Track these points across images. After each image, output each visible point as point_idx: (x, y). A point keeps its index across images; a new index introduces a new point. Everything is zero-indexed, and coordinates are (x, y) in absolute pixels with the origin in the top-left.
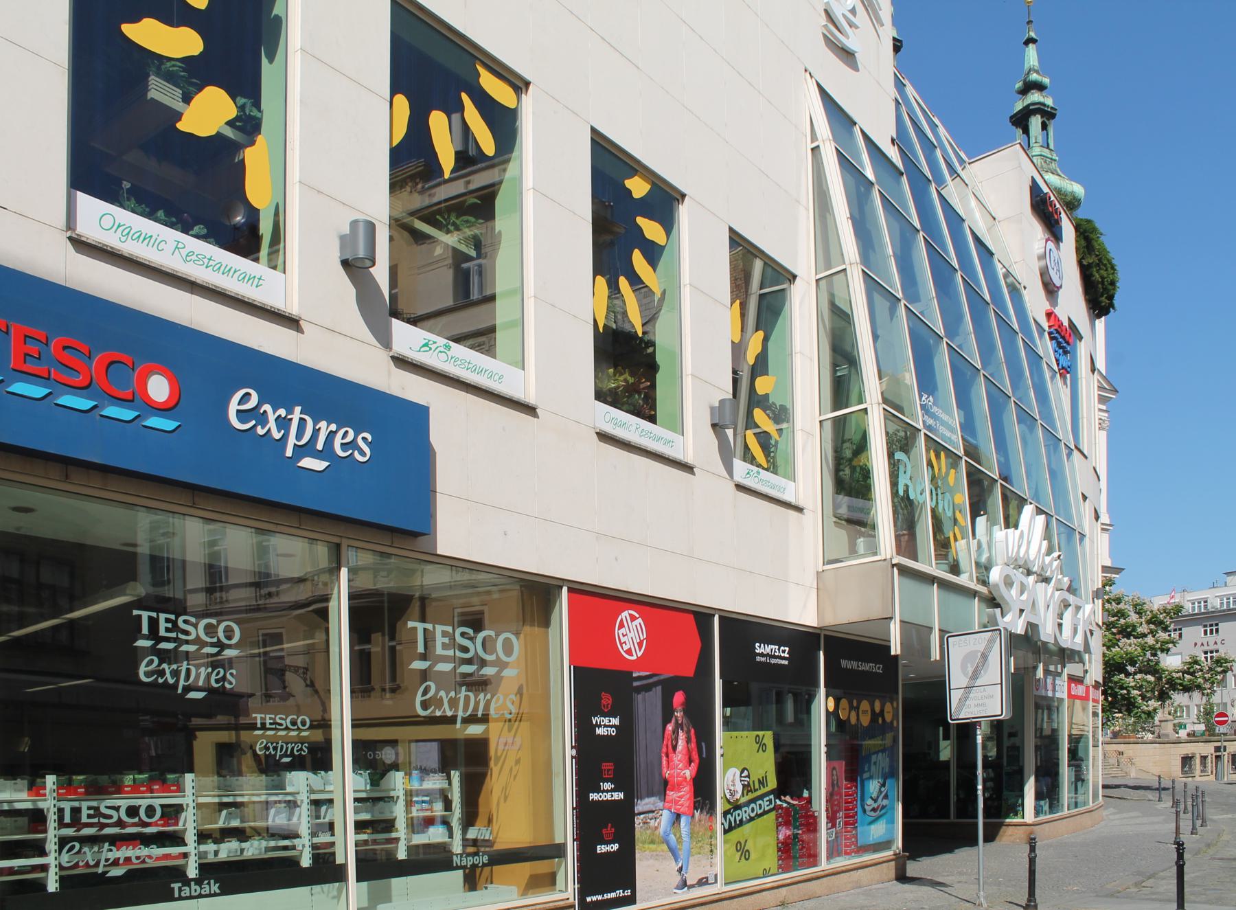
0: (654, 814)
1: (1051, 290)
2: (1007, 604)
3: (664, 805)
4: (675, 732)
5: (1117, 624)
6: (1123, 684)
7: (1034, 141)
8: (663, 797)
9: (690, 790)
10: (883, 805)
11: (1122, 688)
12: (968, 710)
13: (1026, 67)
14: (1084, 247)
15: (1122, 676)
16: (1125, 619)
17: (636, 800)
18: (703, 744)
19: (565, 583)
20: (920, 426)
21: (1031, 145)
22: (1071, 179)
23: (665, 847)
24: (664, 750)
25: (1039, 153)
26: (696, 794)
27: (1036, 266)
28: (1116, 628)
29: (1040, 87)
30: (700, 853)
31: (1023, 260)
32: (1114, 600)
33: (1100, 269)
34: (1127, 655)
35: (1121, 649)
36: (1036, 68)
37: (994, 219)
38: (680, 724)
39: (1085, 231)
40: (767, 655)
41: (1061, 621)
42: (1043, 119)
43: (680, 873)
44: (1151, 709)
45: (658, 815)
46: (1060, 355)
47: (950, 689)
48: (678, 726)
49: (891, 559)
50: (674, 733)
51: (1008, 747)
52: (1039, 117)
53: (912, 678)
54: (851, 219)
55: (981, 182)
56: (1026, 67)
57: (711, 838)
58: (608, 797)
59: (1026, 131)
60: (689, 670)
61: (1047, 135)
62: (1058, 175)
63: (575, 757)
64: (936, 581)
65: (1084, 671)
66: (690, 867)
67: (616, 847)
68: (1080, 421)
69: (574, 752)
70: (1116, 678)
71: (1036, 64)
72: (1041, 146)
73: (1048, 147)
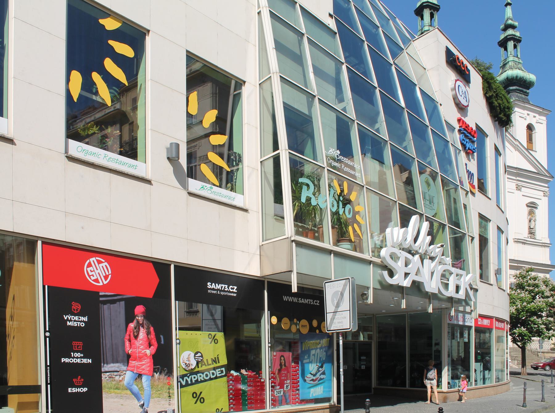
0: (118, 373)
1: (462, 108)
2: (394, 269)
3: (127, 368)
4: (137, 328)
5: (534, 291)
6: (536, 322)
7: (510, 54)
8: (127, 364)
9: (150, 361)
10: (320, 378)
11: (535, 324)
12: (335, 325)
13: (506, 17)
14: (487, 87)
15: (535, 317)
16: (538, 289)
17: (102, 364)
18: (162, 337)
19: (39, 238)
20: (325, 165)
21: (508, 56)
22: (529, 72)
23: (129, 392)
24: (127, 337)
25: (512, 60)
26: (155, 364)
27: (450, 94)
28: (534, 293)
29: (513, 27)
30: (159, 397)
31: (440, 90)
32: (533, 279)
33: (498, 99)
34: (537, 307)
35: (535, 303)
36: (511, 17)
37: (425, 69)
38: (141, 324)
39: (487, 79)
40: (218, 290)
41: (448, 282)
42: (514, 43)
43: (142, 407)
44: (550, 335)
45: (122, 374)
46: (467, 142)
47: (326, 313)
48: (139, 325)
49: (291, 237)
50: (135, 328)
51: (435, 351)
52: (512, 42)
53: (384, 313)
54: (275, 49)
55: (419, 50)
56: (506, 17)
57: (169, 389)
58: (78, 361)
59: (506, 49)
60: (149, 293)
61: (517, 50)
62: (522, 70)
63: (270, 347)
64: (332, 252)
65: (471, 310)
66: (150, 405)
67: (85, 389)
68: (487, 179)
69: (270, 345)
70: (532, 319)
71: (511, 15)
72: (513, 56)
73: (517, 57)
